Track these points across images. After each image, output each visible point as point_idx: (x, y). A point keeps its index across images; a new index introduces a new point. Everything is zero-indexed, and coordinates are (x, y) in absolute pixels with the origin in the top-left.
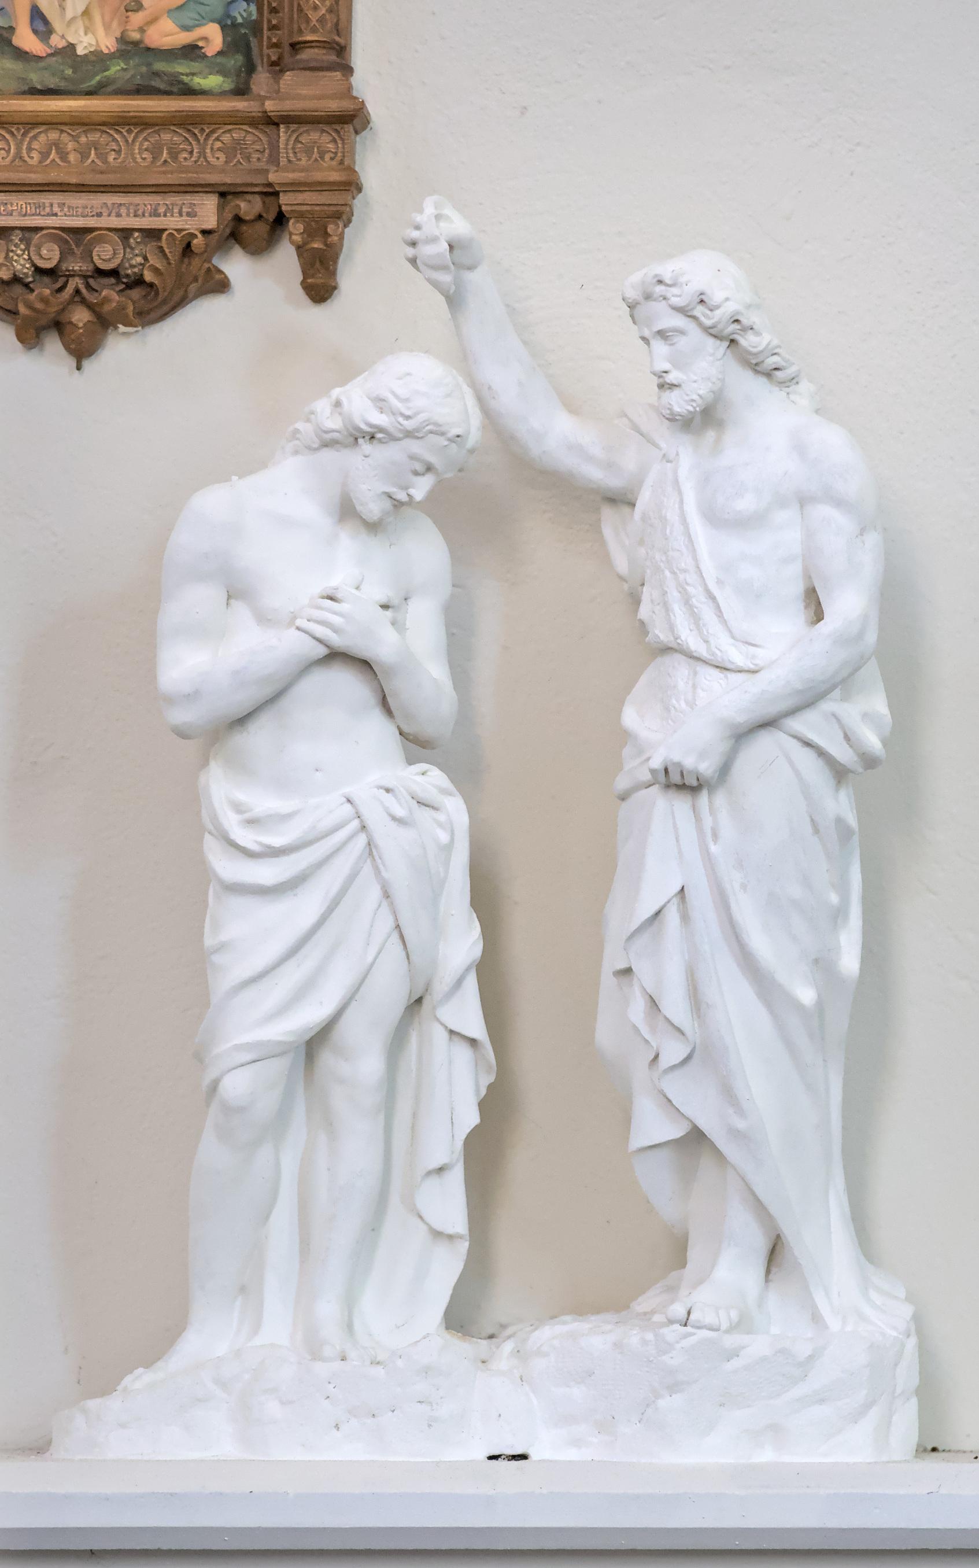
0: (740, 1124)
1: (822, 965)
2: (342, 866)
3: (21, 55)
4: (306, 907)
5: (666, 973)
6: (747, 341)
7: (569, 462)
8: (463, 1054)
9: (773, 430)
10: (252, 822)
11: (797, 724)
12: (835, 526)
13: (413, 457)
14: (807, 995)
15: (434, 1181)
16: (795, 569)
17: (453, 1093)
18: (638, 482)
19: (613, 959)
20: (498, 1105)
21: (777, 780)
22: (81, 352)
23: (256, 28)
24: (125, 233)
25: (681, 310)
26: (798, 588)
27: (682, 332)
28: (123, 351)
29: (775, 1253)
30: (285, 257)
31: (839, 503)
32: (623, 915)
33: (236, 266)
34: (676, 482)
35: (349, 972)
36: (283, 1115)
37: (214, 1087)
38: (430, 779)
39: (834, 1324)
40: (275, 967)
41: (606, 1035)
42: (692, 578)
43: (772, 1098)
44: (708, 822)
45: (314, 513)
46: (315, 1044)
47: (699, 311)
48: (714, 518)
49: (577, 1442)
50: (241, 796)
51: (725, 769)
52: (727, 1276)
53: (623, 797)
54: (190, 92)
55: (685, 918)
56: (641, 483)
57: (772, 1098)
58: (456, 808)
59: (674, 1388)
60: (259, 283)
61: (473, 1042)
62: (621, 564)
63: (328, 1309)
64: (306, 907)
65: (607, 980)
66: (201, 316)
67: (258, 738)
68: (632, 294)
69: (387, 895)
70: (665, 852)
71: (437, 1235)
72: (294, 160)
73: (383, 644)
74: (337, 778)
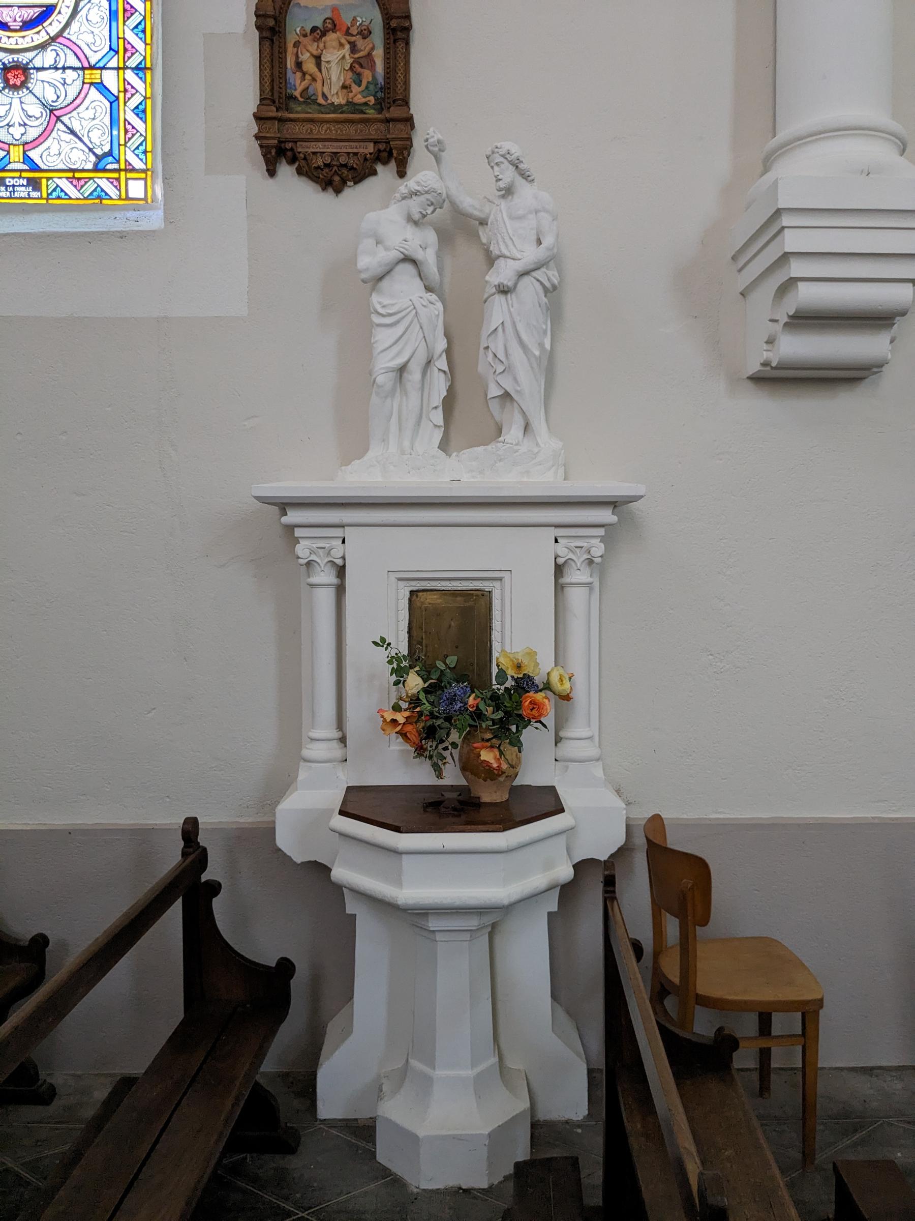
0: (519, 389)
1: (541, 345)
2: (409, 318)
3: (320, 105)
4: (399, 330)
5: (498, 346)
6: (521, 166)
7: (471, 210)
8: (442, 375)
9: (526, 194)
10: (384, 307)
11: (534, 274)
12: (545, 218)
13: (428, 200)
14: (537, 353)
15: (434, 411)
16: (535, 232)
17: (439, 387)
18: (488, 218)
19: (483, 344)
20: (451, 390)
21: (529, 289)
22: (338, 191)
23: (383, 99)
24: (348, 154)
25: (502, 156)
26: (535, 237)
27: (502, 163)
28: (351, 193)
29: (527, 427)
30: (393, 164)
31: (547, 211)
32: (484, 333)
33: (379, 168)
34: (501, 211)
35: (411, 349)
36: (393, 390)
37: (374, 381)
38: (433, 297)
39: (542, 445)
40: (389, 349)
41: (481, 368)
42: (506, 234)
43: (527, 383)
44: (510, 302)
45: (400, 220)
46: (402, 370)
47: (508, 156)
48: (511, 218)
49: (473, 477)
50: (380, 300)
51: (515, 285)
52: (513, 433)
53: (485, 301)
54: (365, 113)
55: (504, 330)
56: (490, 214)
57: (527, 383)
58: (439, 305)
59: (500, 461)
60: (385, 173)
61: (444, 372)
62: (484, 240)
63: (406, 444)
64: (399, 330)
65: (482, 350)
66: (370, 182)
67: (385, 283)
68: (489, 153)
69: (421, 328)
70: (498, 311)
71: (436, 426)
72: (396, 130)
73: (419, 255)
74: (405, 290)
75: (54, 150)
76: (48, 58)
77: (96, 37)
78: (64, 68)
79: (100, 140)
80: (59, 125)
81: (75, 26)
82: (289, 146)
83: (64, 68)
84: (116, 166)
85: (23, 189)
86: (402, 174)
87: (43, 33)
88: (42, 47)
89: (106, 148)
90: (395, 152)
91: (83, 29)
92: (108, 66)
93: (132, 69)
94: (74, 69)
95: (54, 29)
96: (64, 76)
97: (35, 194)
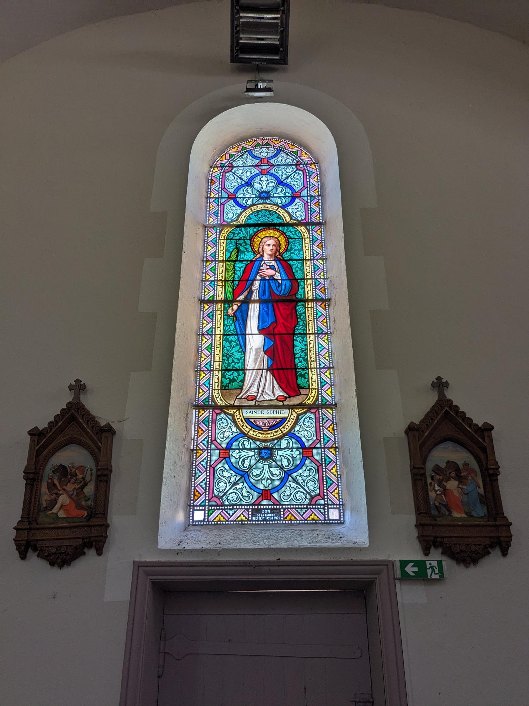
60: (91, 553)
75: (248, 174)
76: (250, 202)
77: (309, 433)
78: (292, 448)
79: (230, 177)
80: (247, 181)
81: (297, 428)
82: (439, 540)
83: (292, 448)
84: (322, 502)
85: (270, 515)
86: (505, 553)
87: (279, 432)
88: (253, 205)
89: (227, 174)
90: (94, 543)
91: (301, 429)
92: (316, 446)
93: (329, 448)
94: (297, 449)
95: (285, 430)
96: (292, 453)
97: (277, 518)
